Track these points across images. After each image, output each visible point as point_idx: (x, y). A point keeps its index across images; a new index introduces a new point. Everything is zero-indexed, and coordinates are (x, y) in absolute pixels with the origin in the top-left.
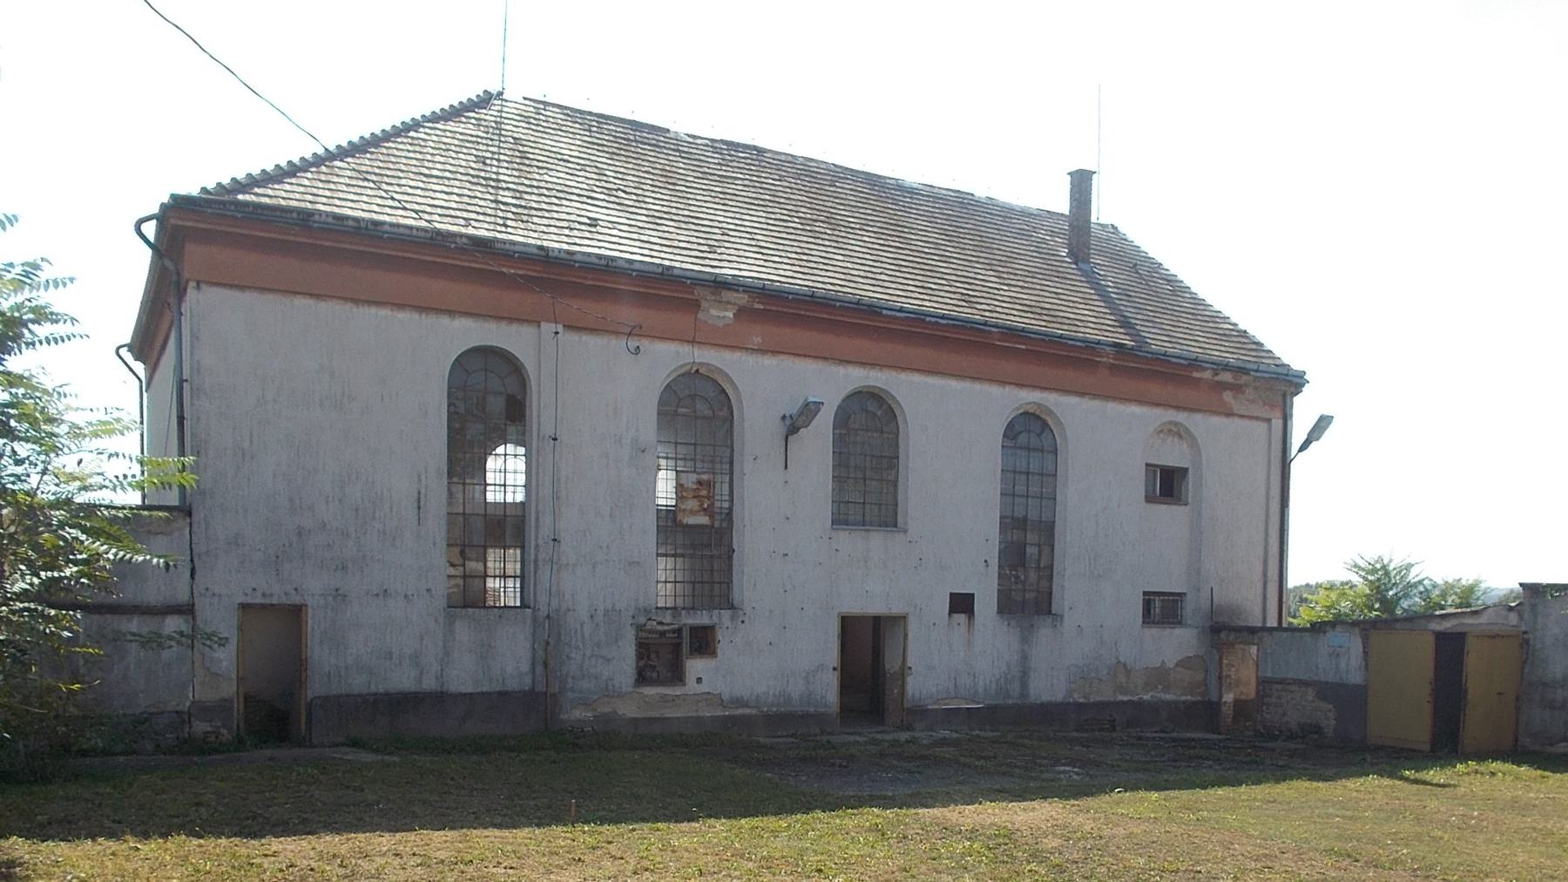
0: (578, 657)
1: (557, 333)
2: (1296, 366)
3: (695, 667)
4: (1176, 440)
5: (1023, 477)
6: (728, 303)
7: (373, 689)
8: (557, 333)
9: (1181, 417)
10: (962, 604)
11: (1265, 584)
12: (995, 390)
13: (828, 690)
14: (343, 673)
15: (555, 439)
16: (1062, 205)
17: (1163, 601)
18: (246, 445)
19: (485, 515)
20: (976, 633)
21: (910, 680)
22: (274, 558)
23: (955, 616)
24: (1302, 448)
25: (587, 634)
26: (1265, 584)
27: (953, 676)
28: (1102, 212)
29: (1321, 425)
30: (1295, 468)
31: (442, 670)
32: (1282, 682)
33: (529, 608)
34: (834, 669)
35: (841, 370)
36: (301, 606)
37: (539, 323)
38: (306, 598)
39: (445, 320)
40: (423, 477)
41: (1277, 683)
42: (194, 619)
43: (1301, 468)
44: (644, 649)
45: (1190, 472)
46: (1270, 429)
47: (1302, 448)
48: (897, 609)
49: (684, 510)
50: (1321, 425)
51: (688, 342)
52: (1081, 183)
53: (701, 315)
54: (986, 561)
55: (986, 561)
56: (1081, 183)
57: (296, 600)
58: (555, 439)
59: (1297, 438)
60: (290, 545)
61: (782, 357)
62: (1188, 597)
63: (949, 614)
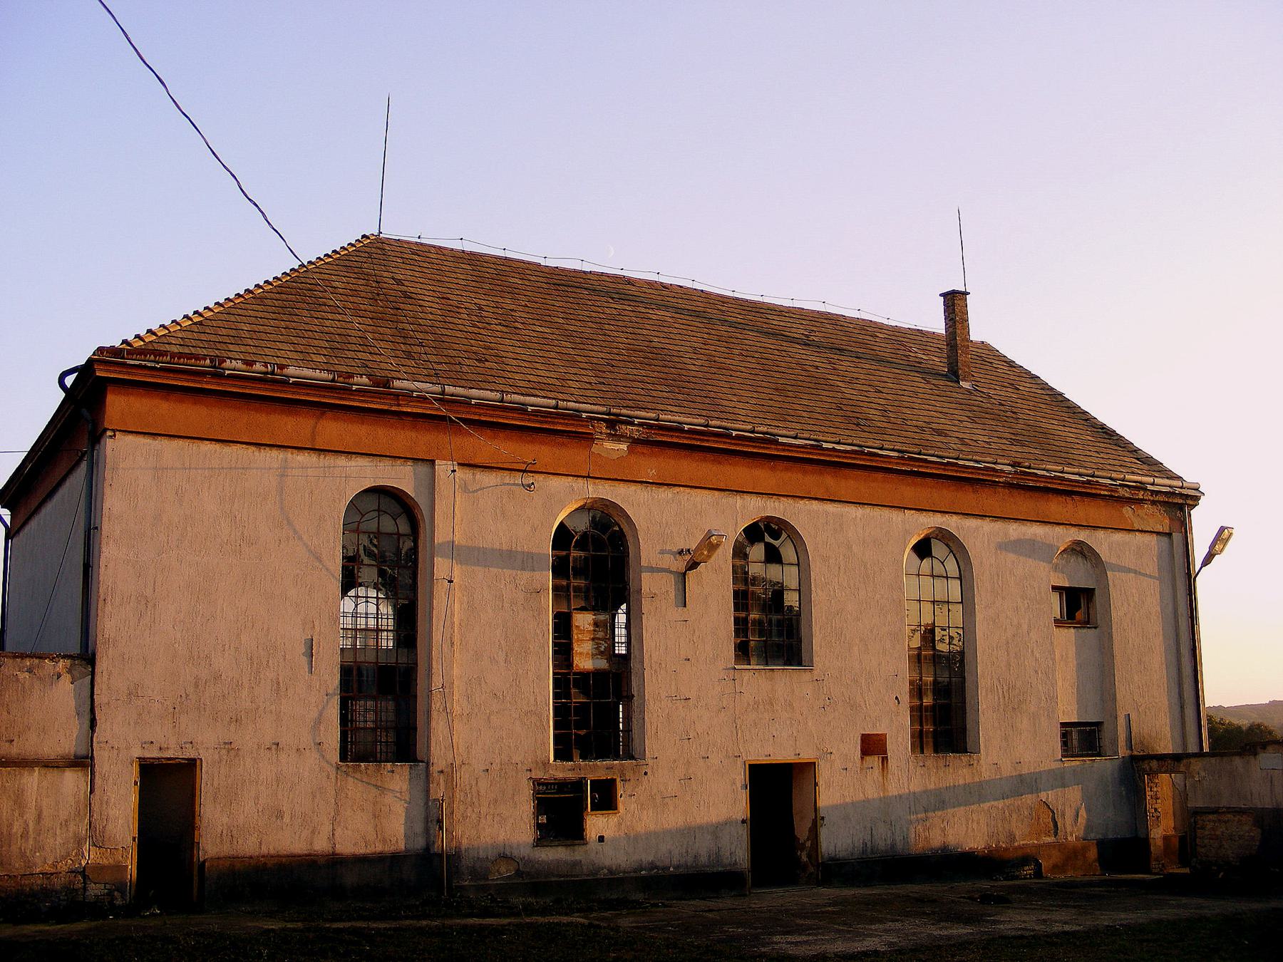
0: (474, 816)
1: (454, 471)
2: (1190, 478)
3: (596, 824)
4: (1080, 559)
5: (930, 606)
6: (622, 436)
7: (264, 850)
8: (454, 471)
9: (1082, 535)
10: (872, 746)
11: (1182, 707)
12: (896, 517)
13: (738, 851)
14: (234, 833)
15: (451, 581)
16: (935, 322)
17: (1079, 731)
18: (149, 592)
19: (377, 663)
20: (890, 776)
21: (824, 833)
22: (172, 710)
23: (867, 758)
24: (1208, 560)
25: (483, 792)
26: (1182, 707)
27: (869, 825)
28: (979, 330)
29: (1221, 538)
30: (1201, 583)
31: (334, 830)
32: (1215, 811)
33: (422, 762)
34: (743, 822)
35: (739, 501)
36: (195, 760)
37: (432, 462)
38: (201, 751)
39: (342, 461)
40: (317, 623)
41: (1209, 813)
42: (93, 773)
43: (1204, 583)
44: (543, 805)
45: (1096, 592)
46: (1171, 544)
47: (1208, 560)
48: (806, 756)
49: (581, 653)
50: (1221, 538)
51: (584, 477)
52: (954, 302)
53: (595, 449)
54: (897, 698)
55: (897, 698)
56: (954, 302)
57: (190, 754)
58: (451, 581)
59: (1199, 552)
60: (187, 695)
61: (677, 489)
62: (1105, 725)
63: (862, 758)
